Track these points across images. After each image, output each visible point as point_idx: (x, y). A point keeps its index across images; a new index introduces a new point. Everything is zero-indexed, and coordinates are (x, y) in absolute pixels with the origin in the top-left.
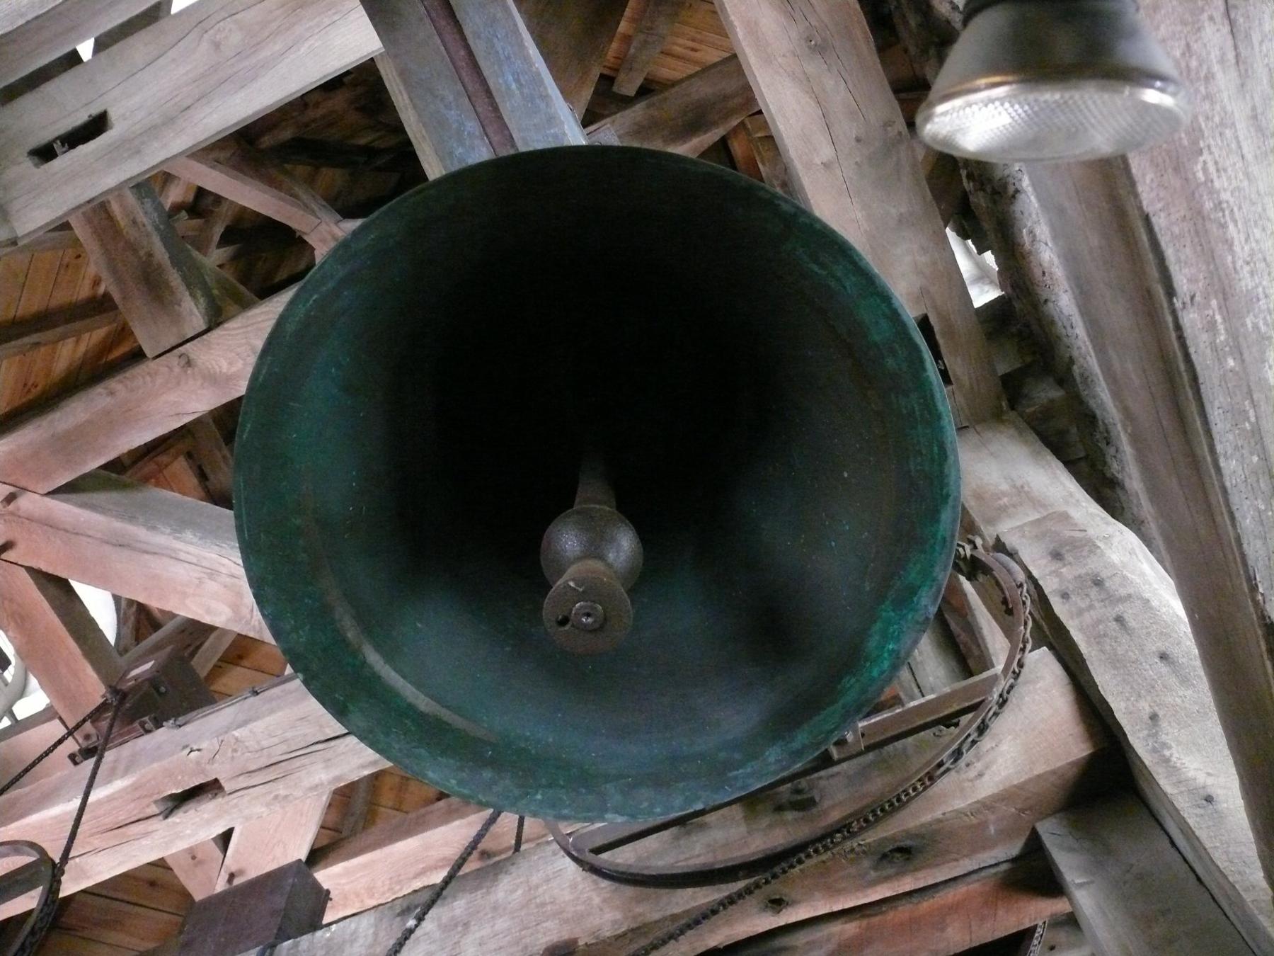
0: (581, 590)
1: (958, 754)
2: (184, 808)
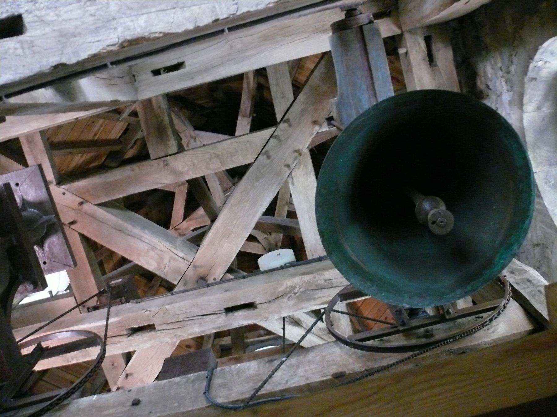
0: (442, 214)
1: (491, 320)
2: (137, 334)
